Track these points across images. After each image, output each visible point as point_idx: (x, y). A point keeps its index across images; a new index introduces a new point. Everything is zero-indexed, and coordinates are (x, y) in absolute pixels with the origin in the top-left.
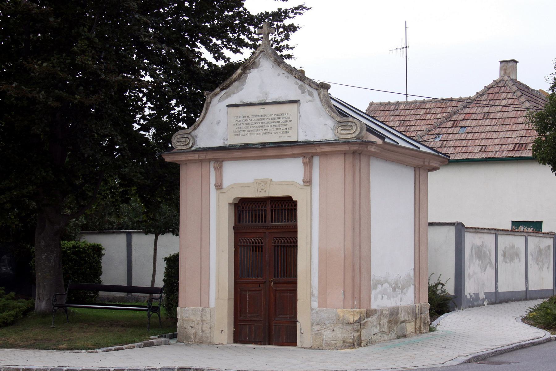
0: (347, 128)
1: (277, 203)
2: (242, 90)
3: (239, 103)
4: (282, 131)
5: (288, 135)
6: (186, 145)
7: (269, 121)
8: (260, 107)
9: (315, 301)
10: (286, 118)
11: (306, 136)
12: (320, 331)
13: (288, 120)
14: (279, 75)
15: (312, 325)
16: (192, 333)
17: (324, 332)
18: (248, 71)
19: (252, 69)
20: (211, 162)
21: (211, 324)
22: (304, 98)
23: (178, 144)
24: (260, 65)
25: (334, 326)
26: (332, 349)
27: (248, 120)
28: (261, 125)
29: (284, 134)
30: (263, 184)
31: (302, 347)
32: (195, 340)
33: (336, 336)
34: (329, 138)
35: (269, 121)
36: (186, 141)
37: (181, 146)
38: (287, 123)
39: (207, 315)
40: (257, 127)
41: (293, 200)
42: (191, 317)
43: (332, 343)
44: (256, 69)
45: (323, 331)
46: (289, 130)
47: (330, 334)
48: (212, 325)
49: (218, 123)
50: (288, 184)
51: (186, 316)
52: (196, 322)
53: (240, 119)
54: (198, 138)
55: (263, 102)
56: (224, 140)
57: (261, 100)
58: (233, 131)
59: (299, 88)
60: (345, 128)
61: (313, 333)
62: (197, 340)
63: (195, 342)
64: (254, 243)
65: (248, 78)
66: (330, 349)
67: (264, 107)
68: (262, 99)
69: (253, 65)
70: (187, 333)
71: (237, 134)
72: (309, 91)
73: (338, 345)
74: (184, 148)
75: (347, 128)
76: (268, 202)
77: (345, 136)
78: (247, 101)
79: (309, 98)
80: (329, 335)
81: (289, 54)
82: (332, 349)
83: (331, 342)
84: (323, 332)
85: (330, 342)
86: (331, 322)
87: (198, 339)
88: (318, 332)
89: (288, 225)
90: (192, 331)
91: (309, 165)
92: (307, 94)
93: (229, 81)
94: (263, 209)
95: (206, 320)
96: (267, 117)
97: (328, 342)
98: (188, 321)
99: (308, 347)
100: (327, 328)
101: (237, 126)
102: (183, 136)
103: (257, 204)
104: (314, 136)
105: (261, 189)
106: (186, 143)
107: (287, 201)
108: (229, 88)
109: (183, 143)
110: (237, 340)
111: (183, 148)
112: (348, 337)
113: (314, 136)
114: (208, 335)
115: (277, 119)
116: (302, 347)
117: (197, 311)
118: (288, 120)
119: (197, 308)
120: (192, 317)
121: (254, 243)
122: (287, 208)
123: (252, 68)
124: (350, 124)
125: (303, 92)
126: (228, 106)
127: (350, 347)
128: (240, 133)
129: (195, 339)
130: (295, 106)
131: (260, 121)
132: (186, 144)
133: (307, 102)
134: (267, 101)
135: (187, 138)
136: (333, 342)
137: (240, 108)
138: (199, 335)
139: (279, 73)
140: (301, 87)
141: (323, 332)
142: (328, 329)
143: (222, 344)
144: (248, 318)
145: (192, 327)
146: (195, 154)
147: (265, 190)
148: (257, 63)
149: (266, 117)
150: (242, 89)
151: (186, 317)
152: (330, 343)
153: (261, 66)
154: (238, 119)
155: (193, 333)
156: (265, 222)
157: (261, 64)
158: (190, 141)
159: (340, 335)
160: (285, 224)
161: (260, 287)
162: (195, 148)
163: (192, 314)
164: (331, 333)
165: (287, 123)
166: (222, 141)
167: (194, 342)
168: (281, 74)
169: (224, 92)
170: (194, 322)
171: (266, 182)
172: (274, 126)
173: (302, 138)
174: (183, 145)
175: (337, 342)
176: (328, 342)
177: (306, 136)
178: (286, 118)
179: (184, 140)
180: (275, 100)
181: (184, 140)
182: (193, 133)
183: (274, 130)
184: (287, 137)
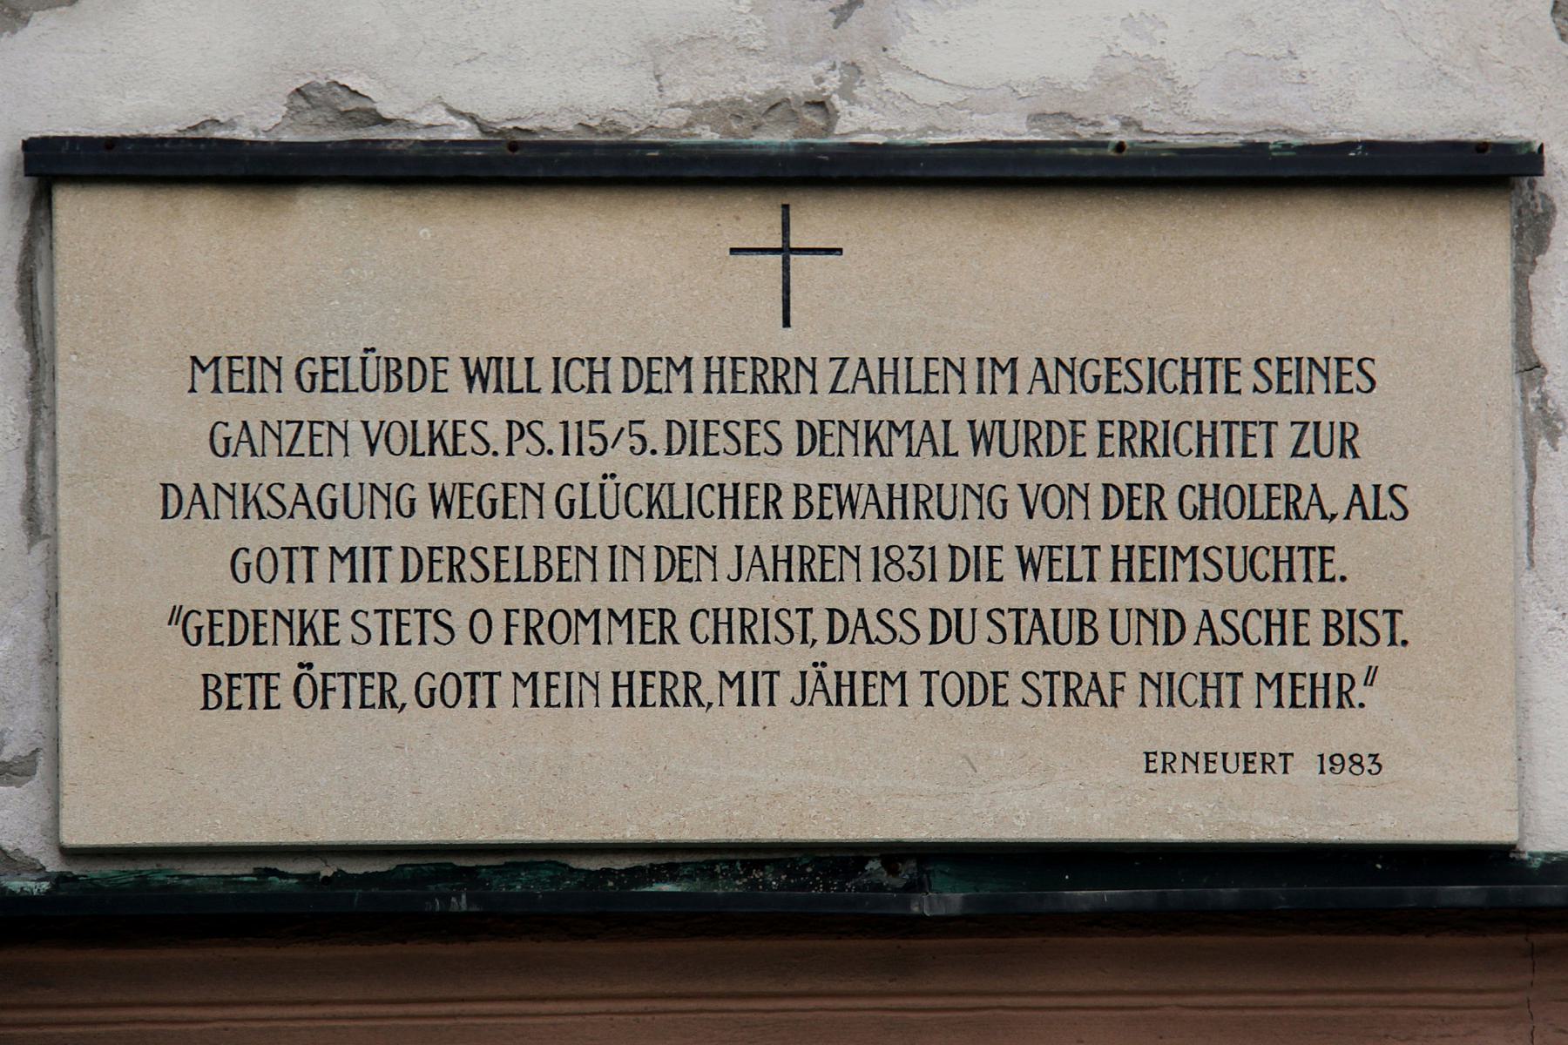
4: (1192, 657)
7: (928, 470)
10: (1284, 438)
27: (496, 433)
35: (928, 470)
38: (1311, 531)
46: (1351, 660)
53: (333, 407)
55: (776, 136)
57: (735, 110)
58: (179, 617)
96: (896, 407)
115: (1089, 444)
128: (324, 660)
131: (737, 470)
149: (862, 406)
165: (1311, 531)
178: (1284, 438)
180: (1037, 118)
184: (1304, 769)
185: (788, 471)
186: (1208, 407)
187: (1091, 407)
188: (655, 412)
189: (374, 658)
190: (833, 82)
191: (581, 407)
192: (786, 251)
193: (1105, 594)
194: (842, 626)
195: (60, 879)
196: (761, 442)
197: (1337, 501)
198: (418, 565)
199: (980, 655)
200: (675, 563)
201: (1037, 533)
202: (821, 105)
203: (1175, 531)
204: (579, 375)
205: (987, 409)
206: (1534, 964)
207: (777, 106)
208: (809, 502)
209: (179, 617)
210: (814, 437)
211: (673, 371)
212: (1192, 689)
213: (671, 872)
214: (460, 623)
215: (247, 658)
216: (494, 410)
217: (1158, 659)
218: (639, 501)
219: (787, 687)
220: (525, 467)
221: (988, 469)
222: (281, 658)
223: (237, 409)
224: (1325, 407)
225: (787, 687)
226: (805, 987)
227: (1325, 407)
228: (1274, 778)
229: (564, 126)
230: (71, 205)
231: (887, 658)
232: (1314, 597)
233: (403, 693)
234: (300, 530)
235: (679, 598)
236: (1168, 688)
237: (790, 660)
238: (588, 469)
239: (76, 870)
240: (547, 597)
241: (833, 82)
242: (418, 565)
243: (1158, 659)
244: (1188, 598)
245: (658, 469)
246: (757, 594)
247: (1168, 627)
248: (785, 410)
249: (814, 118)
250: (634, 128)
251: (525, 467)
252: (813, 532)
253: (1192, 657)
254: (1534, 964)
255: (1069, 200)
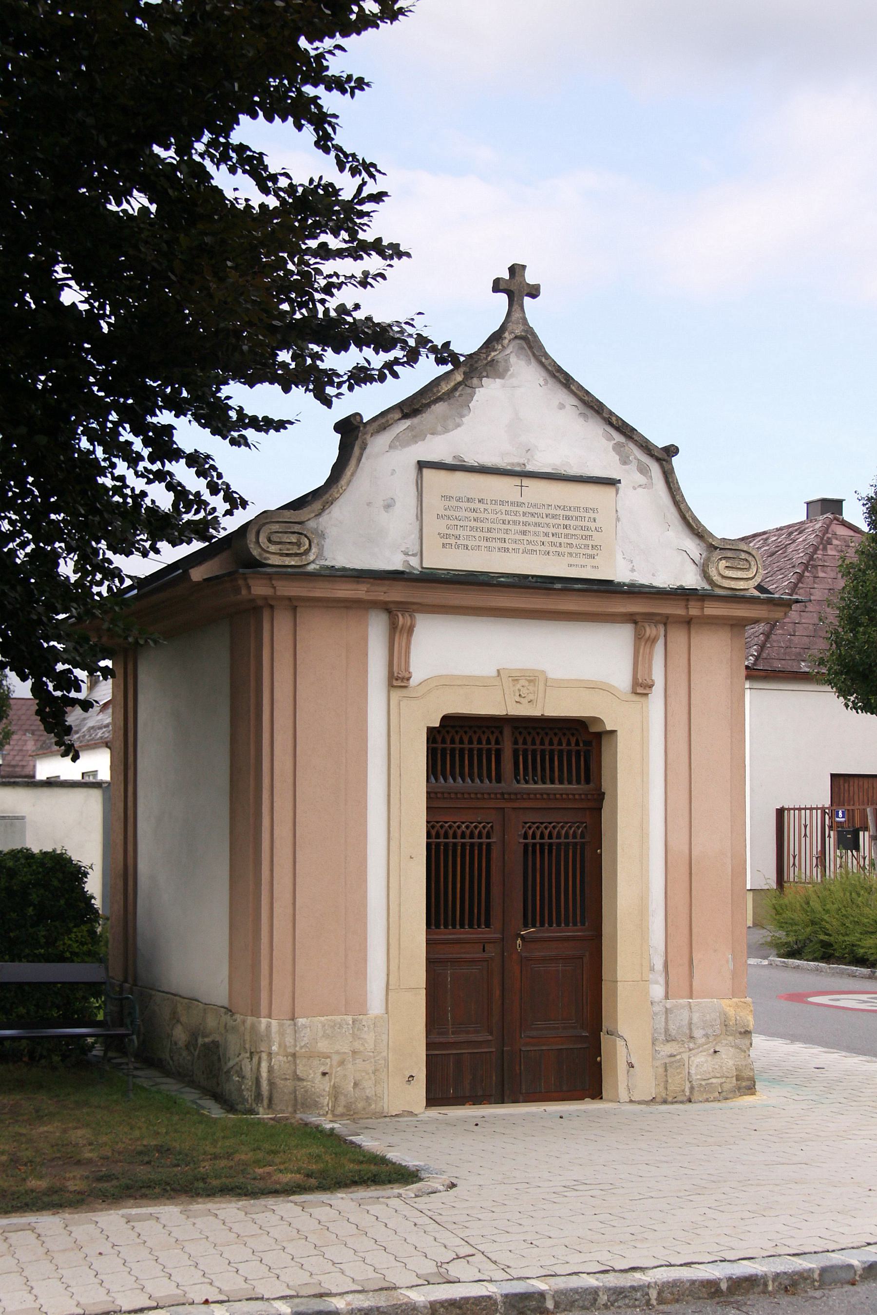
0: (739, 564)
1: (475, 732)
2: (459, 428)
3: (449, 460)
4: (574, 550)
5: (593, 562)
6: (296, 555)
7: (540, 520)
8: (517, 481)
9: (657, 983)
10: (587, 519)
11: (633, 570)
12: (678, 1057)
13: (592, 525)
14: (562, 406)
15: (654, 1042)
16: (324, 1090)
17: (689, 1057)
18: (475, 381)
19: (487, 377)
20: (298, 610)
21: (375, 1062)
22: (629, 476)
23: (273, 548)
24: (509, 373)
25: (715, 1042)
26: (714, 1098)
27: (482, 510)
28: (521, 528)
29: (583, 561)
30: (523, 682)
31: (631, 1101)
32: (333, 1111)
33: (721, 1067)
34: (688, 584)
35: (540, 520)
36: (298, 544)
37: (281, 555)
38: (590, 533)
39: (366, 1036)
40: (507, 531)
41: (438, 725)
42: (319, 1044)
43: (712, 1083)
44: (497, 380)
45: (685, 1056)
46: (595, 552)
47: (707, 1061)
48: (380, 1062)
49: (388, 507)
50: (593, 687)
51: (302, 1044)
52: (336, 1058)
53: (460, 504)
54: (327, 540)
55: (518, 469)
56: (406, 554)
57: (513, 464)
58: (439, 534)
59: (614, 449)
60: (736, 563)
61: (658, 1063)
62: (340, 1110)
63: (334, 1115)
64: (546, 837)
65: (475, 398)
66: (710, 1100)
67: (526, 482)
68: (516, 460)
69: (488, 368)
70: (306, 1091)
71: (448, 541)
72: (638, 460)
73: (727, 1087)
74: (293, 563)
75: (739, 564)
76: (507, 732)
77: (733, 583)
78: (472, 459)
79: (640, 479)
80: (705, 1065)
81: (346, 352)
82: (714, 1098)
83: (710, 1081)
84: (686, 1060)
85: (706, 1082)
86: (710, 1031)
87: (345, 1106)
88: (673, 1059)
89: (569, 792)
90: (323, 1086)
91: (642, 643)
92: (633, 466)
93: (430, 398)
94: (493, 746)
95: (361, 1052)
96: (536, 511)
97: (703, 1083)
98: (310, 1056)
99: (646, 1100)
100: (699, 1047)
101: (449, 522)
102: (290, 528)
103: (484, 732)
104: (653, 575)
105: (520, 695)
106: (299, 549)
107: (556, 731)
108: (419, 416)
109: (288, 546)
110: (434, 1099)
111: (287, 563)
112: (746, 1066)
113: (653, 575)
114: (369, 1092)
115: (561, 518)
116: (631, 1101)
117: (341, 1027)
118: (592, 525)
119: (338, 1018)
120: (323, 1046)
121: (546, 837)
122: (573, 747)
123: (485, 374)
124: (743, 556)
125: (625, 461)
126: (422, 465)
127: (749, 1089)
128: (459, 542)
129: (334, 1107)
130: (609, 491)
131: (515, 518)
132: (298, 552)
133: (634, 488)
134: (530, 468)
135: (306, 536)
136: (714, 1081)
137: (459, 475)
138: (346, 1096)
139: (562, 401)
140: (618, 448)
141: (686, 1060)
142: (701, 1049)
143: (411, 1114)
144: (452, 1038)
145: (324, 1074)
146: (358, 582)
147: (531, 697)
148: (502, 365)
149: (532, 510)
150: (459, 425)
151: (301, 1048)
152: (707, 1084)
153: (512, 376)
154: (454, 503)
155: (327, 1089)
156: (499, 780)
157: (511, 369)
158: (310, 545)
159: (731, 1063)
160: (562, 789)
161: (484, 951)
162: (318, 567)
163: (323, 1036)
164: (709, 1059)
165: (590, 533)
166: (403, 557)
167: (330, 1116)
168: (568, 407)
169: (407, 423)
170: (328, 1060)
171: (532, 678)
172: (553, 535)
173: (621, 574)
174: (287, 555)
175: (723, 1080)
176: (703, 1083)
177: (633, 570)
178: (587, 519)
179: (294, 541)
180: (553, 469)
181: (293, 538)
182: (312, 524)
183: (553, 544)
184: (589, 568)
185: (522, 519)
186: (577, 514)
187: (562, 513)
188: (504, 508)
189: (465, 542)
190: (526, 461)
191: (494, 507)
192: (522, 486)
193: (563, 540)
194: (529, 542)
195: (421, 572)
196: (518, 514)
197: (593, 529)
198: (472, 529)
199: (547, 548)
200: (507, 531)
201: (554, 531)
202: (524, 464)
203: (572, 532)
204: (493, 502)
205: (548, 512)
206: (687, 605)
207: (519, 464)
208: (525, 524)
209: (439, 534)
210: (524, 514)
211: (807, 610)
212: (574, 555)
213: (503, 577)
214: (477, 538)
215: (448, 541)
216: (482, 506)
217: (570, 550)
218: (501, 522)
219: (521, 551)
220: (486, 515)
221: (548, 520)
222: (453, 541)
223: (448, 503)
224: (591, 515)
225: (521, 551)
226: (346, 588)
227: (591, 515)
228: (585, 569)
229: (489, 465)
230: (426, 472)
231: (534, 548)
232: (590, 543)
233: (469, 548)
234: (456, 522)
235: (506, 536)
236: (570, 554)
237: (521, 547)
238: (495, 516)
239: (423, 570)
240: (489, 535)
241: (526, 461)
242: (472, 529)
243: (570, 550)
244: (574, 542)
245: (504, 517)
246: (518, 537)
247: (570, 545)
248: (521, 510)
249: (523, 466)
250: (499, 466)
251: (486, 515)
252: (525, 528)
253: (574, 550)
254: (687, 605)
255: (559, 481)
